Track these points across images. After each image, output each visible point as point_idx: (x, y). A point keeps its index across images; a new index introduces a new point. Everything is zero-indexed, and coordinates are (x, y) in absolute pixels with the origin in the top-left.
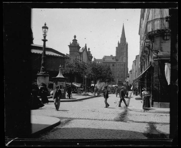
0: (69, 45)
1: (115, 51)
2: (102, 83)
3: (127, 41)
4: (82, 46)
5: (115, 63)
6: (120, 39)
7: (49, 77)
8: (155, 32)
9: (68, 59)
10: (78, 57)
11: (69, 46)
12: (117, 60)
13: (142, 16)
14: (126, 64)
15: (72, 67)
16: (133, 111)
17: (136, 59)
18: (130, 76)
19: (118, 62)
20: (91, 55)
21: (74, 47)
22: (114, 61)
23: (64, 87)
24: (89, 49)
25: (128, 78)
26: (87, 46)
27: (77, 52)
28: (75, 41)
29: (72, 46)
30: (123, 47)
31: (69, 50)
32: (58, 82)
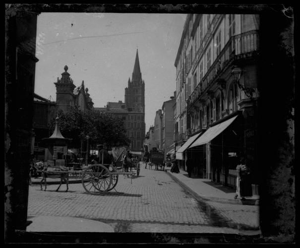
0: (56, 81)
1: (124, 94)
2: (121, 149)
3: (144, 78)
4: (77, 84)
5: (127, 114)
6: (132, 74)
7: (35, 137)
8: (248, 55)
9: (53, 107)
10: (72, 104)
11: (55, 83)
12: (130, 110)
13: (188, 33)
14: (142, 116)
15: (70, 119)
16: (211, 201)
17: (163, 107)
18: (151, 136)
19: (131, 112)
20: (91, 100)
21: (65, 85)
22: (125, 111)
23: (65, 156)
24: (87, 90)
25: (146, 140)
26: (85, 84)
27: (71, 94)
28: (66, 75)
29: (61, 85)
30: (136, 88)
31: (56, 91)
32: (54, 147)
